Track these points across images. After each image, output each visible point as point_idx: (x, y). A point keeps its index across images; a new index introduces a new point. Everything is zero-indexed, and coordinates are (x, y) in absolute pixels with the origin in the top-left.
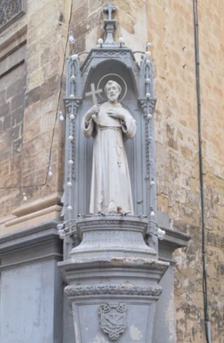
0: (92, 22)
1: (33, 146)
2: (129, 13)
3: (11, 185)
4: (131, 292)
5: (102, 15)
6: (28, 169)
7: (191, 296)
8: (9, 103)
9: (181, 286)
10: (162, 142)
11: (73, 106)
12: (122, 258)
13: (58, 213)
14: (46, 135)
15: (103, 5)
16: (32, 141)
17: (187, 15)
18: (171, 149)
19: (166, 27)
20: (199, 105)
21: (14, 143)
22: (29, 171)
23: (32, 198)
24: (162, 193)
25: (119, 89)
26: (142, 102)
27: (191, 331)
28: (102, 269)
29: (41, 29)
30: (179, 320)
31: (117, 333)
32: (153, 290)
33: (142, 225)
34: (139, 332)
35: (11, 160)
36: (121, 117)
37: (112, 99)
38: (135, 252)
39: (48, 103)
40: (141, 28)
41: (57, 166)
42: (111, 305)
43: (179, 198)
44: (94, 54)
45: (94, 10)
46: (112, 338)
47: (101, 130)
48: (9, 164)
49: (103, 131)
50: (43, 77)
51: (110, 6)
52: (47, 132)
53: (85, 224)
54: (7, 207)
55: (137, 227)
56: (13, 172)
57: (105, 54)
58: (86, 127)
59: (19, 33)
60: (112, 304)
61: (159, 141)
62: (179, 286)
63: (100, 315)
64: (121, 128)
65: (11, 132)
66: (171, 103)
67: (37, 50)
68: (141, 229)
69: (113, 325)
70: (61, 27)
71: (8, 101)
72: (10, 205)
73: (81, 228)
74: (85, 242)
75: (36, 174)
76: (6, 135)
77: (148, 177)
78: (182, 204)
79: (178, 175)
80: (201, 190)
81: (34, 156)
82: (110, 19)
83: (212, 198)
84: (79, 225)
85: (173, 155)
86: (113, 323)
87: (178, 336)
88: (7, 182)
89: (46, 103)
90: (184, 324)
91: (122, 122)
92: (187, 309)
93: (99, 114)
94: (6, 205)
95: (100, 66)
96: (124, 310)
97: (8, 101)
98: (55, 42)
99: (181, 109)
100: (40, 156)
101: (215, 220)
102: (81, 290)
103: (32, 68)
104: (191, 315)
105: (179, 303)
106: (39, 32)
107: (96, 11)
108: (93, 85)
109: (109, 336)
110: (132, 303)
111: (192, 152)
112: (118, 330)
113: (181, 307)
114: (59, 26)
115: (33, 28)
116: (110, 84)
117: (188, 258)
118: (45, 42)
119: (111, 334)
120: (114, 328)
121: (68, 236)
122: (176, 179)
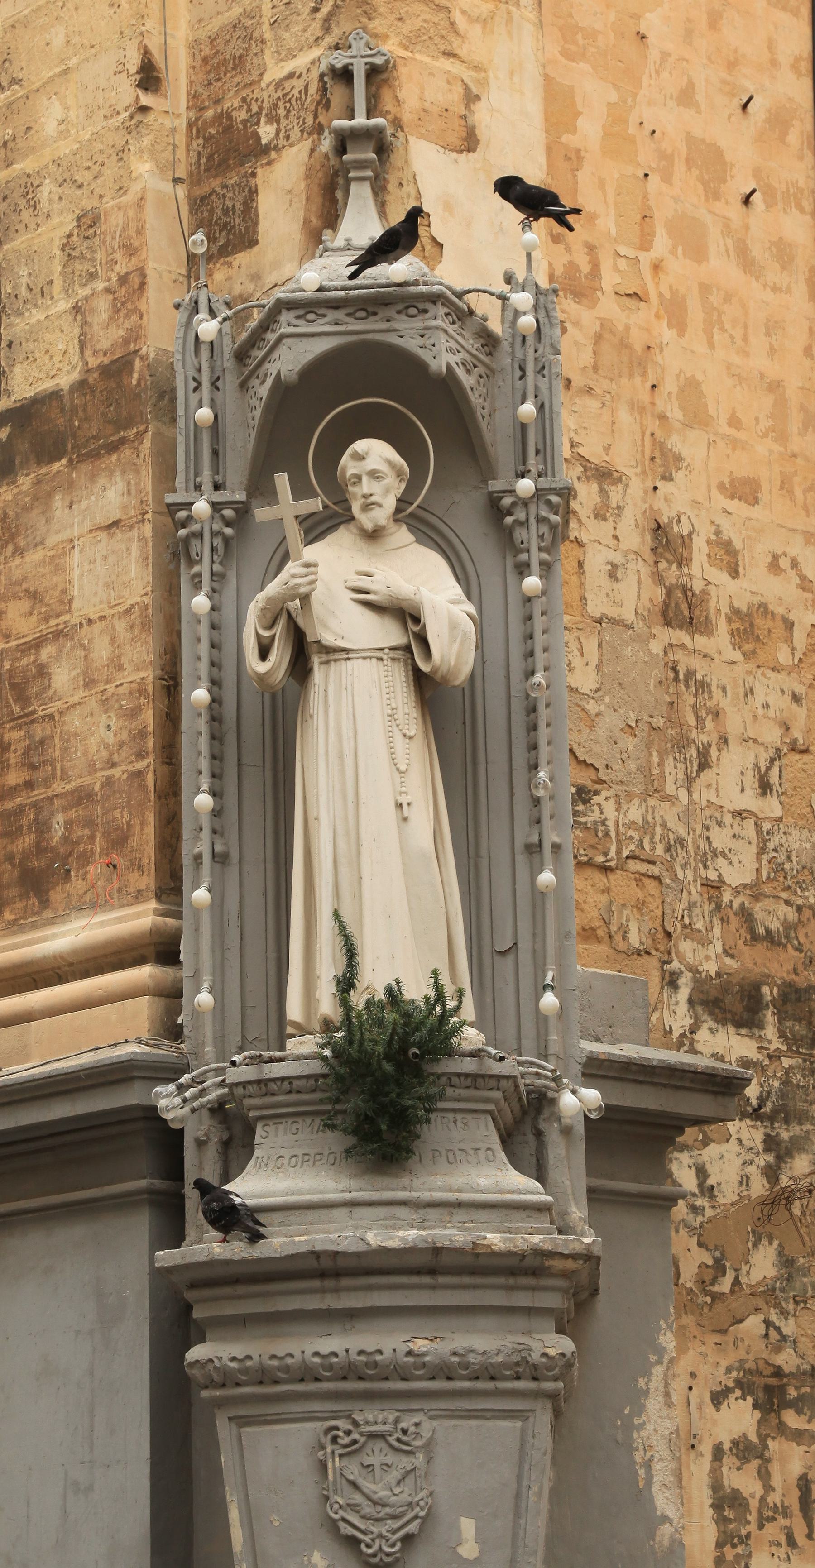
0: (282, 112)
1: (42, 671)
2: (450, 54)
4: (444, 1371)
5: (323, 90)
7: (789, 1328)
9: (736, 1282)
10: (629, 616)
13: (160, 1002)
14: (98, 626)
15: (329, 40)
16: (37, 644)
18: (680, 636)
22: (29, 785)
23: (48, 914)
24: (632, 857)
25: (399, 474)
27: (795, 1494)
30: (726, 1446)
31: (394, 1538)
32: (535, 1357)
33: (493, 1083)
36: (404, 605)
37: (367, 520)
39: (102, 481)
41: (150, 780)
42: (367, 1423)
43: (721, 862)
44: (287, 323)
46: (374, 1555)
47: (327, 662)
51: (358, 47)
52: (102, 618)
55: (472, 1092)
58: (264, 654)
60: (370, 1418)
61: (612, 612)
62: (725, 1285)
64: (408, 649)
66: (675, 414)
67: (44, 206)
68: (487, 1100)
69: (375, 1503)
70: (150, 118)
73: (247, 1102)
74: (263, 1165)
75: (58, 802)
77: (535, 839)
78: (736, 891)
79: (714, 752)
81: (51, 717)
82: (360, 120)
84: (239, 1091)
85: (684, 662)
86: (375, 1497)
87: (721, 1520)
89: (93, 477)
90: (755, 1464)
91: (411, 626)
92: (769, 1390)
93: (316, 597)
96: (418, 1443)
98: (122, 190)
99: (734, 421)
100: (75, 722)
102: (249, 1363)
103: (24, 293)
104: (791, 1419)
105: (724, 1364)
108: (282, 481)
109: (363, 1546)
112: (397, 1524)
113: (739, 1383)
114: (138, 117)
116: (359, 457)
117: (771, 1143)
119: (367, 1539)
120: (380, 1515)
121: (205, 1113)
122: (707, 776)
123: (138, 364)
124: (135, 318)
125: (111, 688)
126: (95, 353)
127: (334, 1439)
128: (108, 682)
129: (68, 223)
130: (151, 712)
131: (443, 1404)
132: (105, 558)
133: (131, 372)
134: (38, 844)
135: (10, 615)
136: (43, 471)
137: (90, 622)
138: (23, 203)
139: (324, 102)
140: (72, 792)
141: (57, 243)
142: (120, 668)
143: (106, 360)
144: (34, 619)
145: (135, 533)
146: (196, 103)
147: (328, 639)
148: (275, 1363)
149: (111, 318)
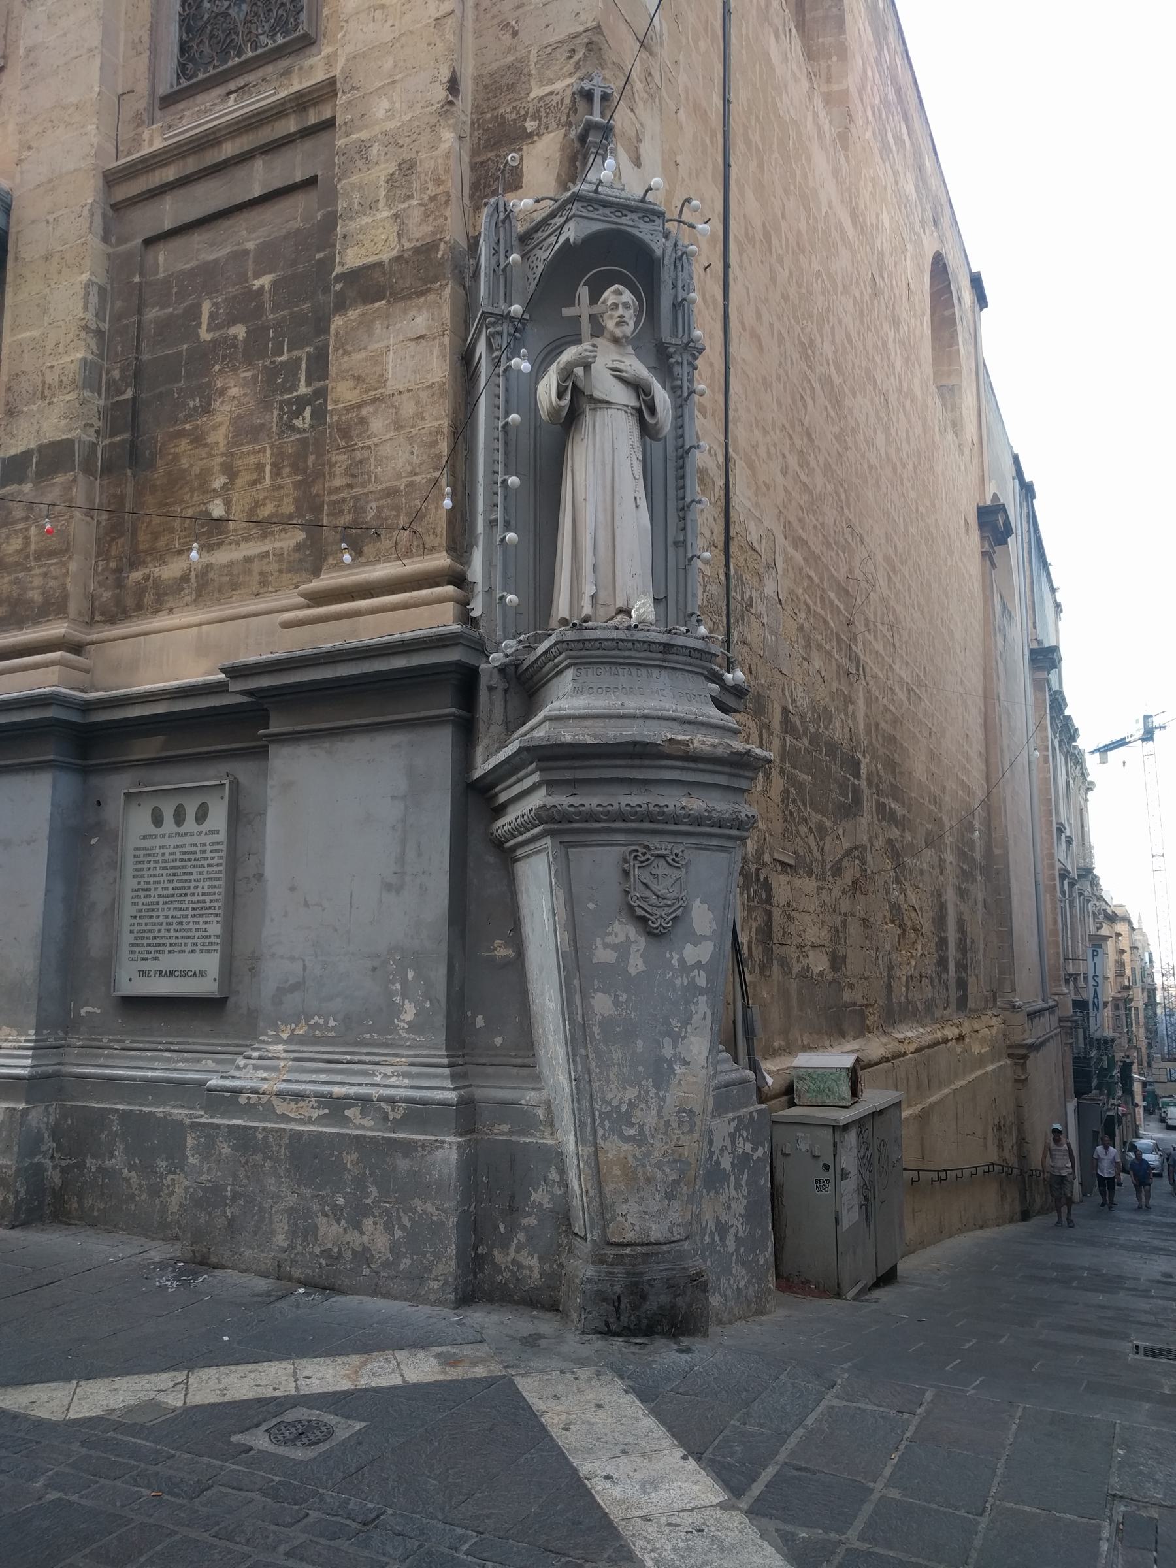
0: (543, 114)
1: (362, 421)
2: (632, 110)
3: (270, 516)
4: (698, 821)
5: (574, 102)
6: (347, 480)
8: (263, 287)
11: (505, 334)
12: (687, 738)
14: (405, 396)
15: (578, 74)
17: (713, 136)
19: (679, 159)
20: (727, 368)
21: (281, 403)
22: (350, 486)
23: (363, 559)
26: (672, 349)
28: (637, 762)
29: (385, 104)
34: (711, 915)
35: (272, 446)
38: (703, 724)
40: (650, 151)
45: (551, 82)
47: (595, 409)
48: (267, 459)
49: (599, 413)
50: (393, 239)
53: (580, 645)
54: (261, 573)
55: (699, 662)
56: (280, 482)
57: (602, 211)
59: (302, 96)
63: (626, 873)
65: (273, 372)
70: (454, 109)
71: (258, 283)
72: (276, 566)
76: (254, 377)
80: (727, 575)
81: (369, 447)
82: (597, 118)
83: (743, 599)
88: (258, 504)
89: (405, 312)
94: (256, 566)
95: (591, 240)
97: (258, 283)
98: (434, 148)
100: (387, 449)
101: (747, 649)
103: (356, 207)
106: (380, 108)
107: (559, 86)
110: (699, 847)
111: (714, 483)
115: (357, 94)
118: (401, 142)
119: (653, 918)
123: (442, 246)
124: (442, 220)
125: (415, 431)
126: (410, 240)
127: (635, 857)
128: (412, 427)
129: (392, 167)
130: (445, 444)
131: (693, 840)
132: (413, 356)
133: (438, 250)
134: (355, 521)
135: (339, 389)
136: (369, 307)
137: (400, 393)
138: (357, 157)
139: (573, 109)
140: (383, 490)
141: (383, 178)
142: (423, 418)
143: (418, 244)
144: (358, 391)
145: (437, 341)
146: (477, 109)
147: (598, 394)
148: (600, 809)
149: (422, 220)
